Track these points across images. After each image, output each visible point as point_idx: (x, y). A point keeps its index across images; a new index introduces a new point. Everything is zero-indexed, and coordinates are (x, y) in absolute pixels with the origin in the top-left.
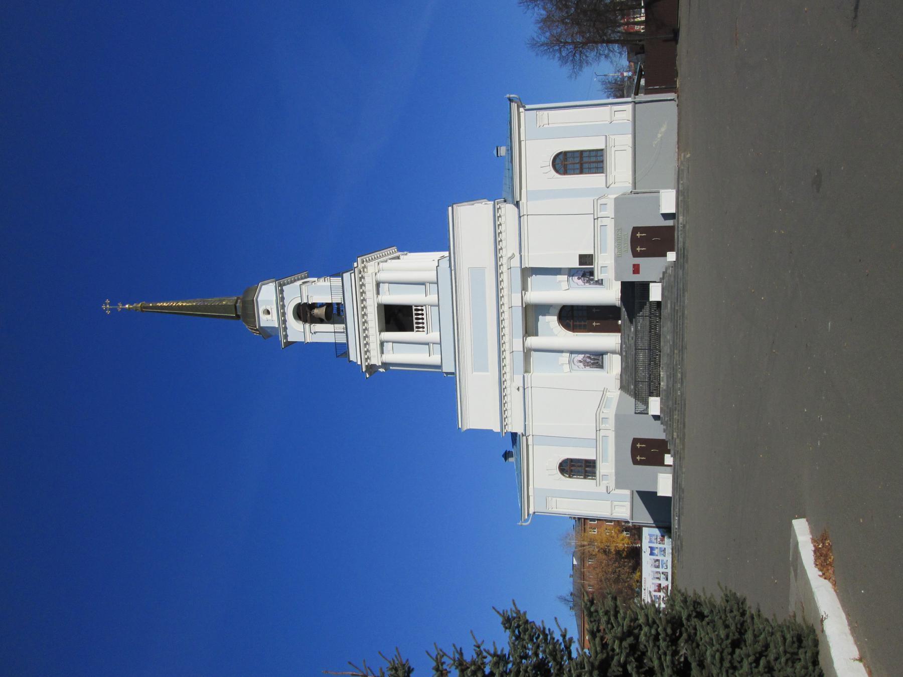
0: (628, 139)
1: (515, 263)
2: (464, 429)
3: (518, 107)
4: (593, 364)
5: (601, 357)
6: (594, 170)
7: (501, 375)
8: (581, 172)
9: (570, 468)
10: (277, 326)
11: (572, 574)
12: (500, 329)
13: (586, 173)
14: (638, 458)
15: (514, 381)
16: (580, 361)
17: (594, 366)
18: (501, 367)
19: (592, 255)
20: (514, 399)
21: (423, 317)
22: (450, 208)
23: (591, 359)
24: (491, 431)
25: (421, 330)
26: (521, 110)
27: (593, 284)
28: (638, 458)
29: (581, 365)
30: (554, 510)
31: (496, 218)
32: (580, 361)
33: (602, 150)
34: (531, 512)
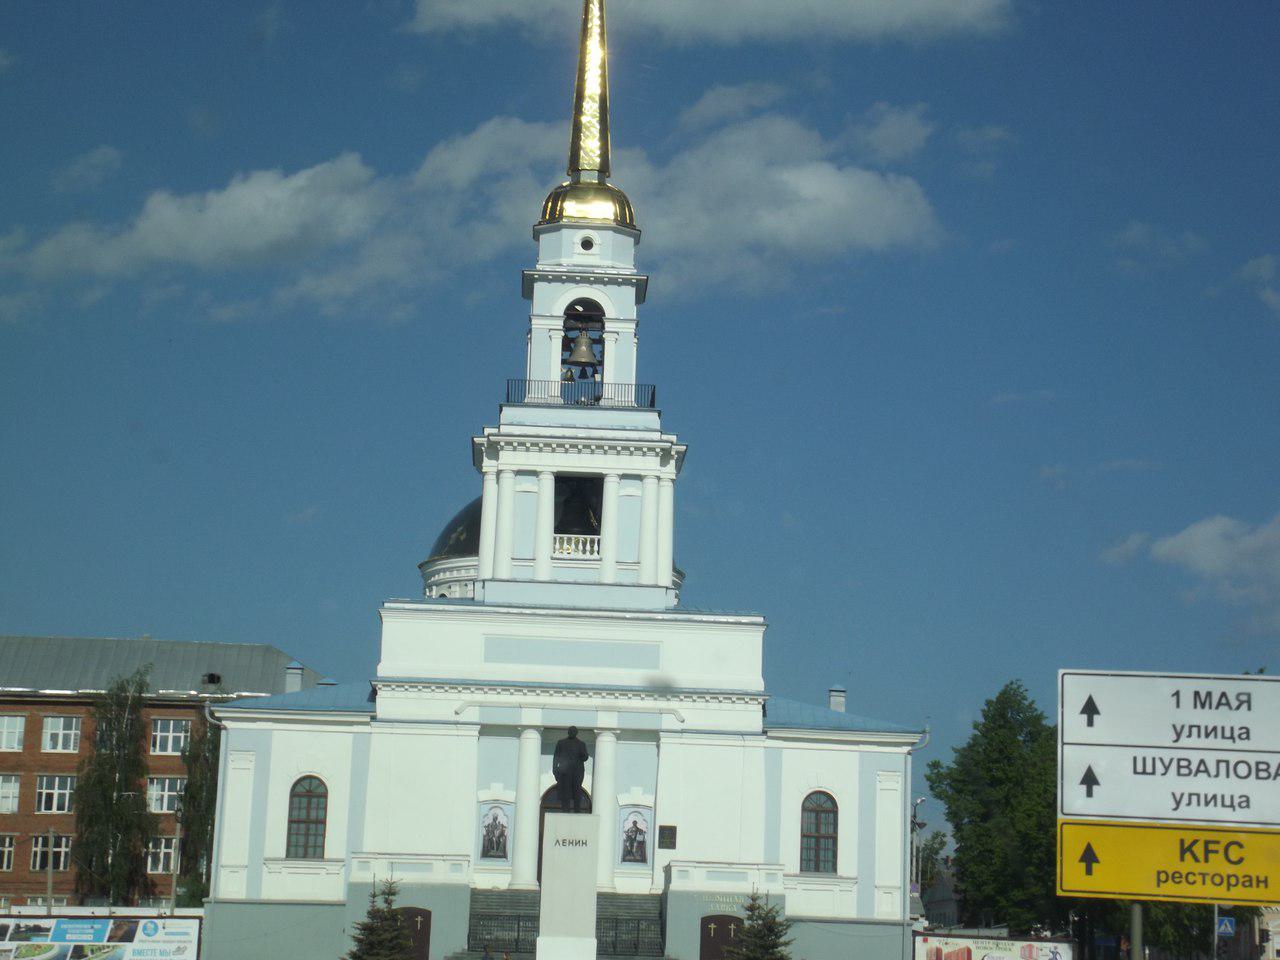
0: (851, 912)
1: (668, 722)
2: (383, 614)
3: (913, 744)
4: (490, 840)
5: (638, 858)
8: (323, 822)
9: (309, 798)
10: (538, 267)
13: (802, 842)
14: (713, 926)
15: (472, 707)
16: (495, 819)
17: (486, 843)
19: (660, 847)
20: (442, 705)
21: (588, 553)
22: (761, 620)
23: (499, 837)
24: (379, 661)
25: (558, 546)
26: (906, 749)
27: (625, 847)
29: (489, 821)
30: (231, 765)
31: (742, 696)
32: (495, 819)
33: (835, 869)
34: (224, 723)
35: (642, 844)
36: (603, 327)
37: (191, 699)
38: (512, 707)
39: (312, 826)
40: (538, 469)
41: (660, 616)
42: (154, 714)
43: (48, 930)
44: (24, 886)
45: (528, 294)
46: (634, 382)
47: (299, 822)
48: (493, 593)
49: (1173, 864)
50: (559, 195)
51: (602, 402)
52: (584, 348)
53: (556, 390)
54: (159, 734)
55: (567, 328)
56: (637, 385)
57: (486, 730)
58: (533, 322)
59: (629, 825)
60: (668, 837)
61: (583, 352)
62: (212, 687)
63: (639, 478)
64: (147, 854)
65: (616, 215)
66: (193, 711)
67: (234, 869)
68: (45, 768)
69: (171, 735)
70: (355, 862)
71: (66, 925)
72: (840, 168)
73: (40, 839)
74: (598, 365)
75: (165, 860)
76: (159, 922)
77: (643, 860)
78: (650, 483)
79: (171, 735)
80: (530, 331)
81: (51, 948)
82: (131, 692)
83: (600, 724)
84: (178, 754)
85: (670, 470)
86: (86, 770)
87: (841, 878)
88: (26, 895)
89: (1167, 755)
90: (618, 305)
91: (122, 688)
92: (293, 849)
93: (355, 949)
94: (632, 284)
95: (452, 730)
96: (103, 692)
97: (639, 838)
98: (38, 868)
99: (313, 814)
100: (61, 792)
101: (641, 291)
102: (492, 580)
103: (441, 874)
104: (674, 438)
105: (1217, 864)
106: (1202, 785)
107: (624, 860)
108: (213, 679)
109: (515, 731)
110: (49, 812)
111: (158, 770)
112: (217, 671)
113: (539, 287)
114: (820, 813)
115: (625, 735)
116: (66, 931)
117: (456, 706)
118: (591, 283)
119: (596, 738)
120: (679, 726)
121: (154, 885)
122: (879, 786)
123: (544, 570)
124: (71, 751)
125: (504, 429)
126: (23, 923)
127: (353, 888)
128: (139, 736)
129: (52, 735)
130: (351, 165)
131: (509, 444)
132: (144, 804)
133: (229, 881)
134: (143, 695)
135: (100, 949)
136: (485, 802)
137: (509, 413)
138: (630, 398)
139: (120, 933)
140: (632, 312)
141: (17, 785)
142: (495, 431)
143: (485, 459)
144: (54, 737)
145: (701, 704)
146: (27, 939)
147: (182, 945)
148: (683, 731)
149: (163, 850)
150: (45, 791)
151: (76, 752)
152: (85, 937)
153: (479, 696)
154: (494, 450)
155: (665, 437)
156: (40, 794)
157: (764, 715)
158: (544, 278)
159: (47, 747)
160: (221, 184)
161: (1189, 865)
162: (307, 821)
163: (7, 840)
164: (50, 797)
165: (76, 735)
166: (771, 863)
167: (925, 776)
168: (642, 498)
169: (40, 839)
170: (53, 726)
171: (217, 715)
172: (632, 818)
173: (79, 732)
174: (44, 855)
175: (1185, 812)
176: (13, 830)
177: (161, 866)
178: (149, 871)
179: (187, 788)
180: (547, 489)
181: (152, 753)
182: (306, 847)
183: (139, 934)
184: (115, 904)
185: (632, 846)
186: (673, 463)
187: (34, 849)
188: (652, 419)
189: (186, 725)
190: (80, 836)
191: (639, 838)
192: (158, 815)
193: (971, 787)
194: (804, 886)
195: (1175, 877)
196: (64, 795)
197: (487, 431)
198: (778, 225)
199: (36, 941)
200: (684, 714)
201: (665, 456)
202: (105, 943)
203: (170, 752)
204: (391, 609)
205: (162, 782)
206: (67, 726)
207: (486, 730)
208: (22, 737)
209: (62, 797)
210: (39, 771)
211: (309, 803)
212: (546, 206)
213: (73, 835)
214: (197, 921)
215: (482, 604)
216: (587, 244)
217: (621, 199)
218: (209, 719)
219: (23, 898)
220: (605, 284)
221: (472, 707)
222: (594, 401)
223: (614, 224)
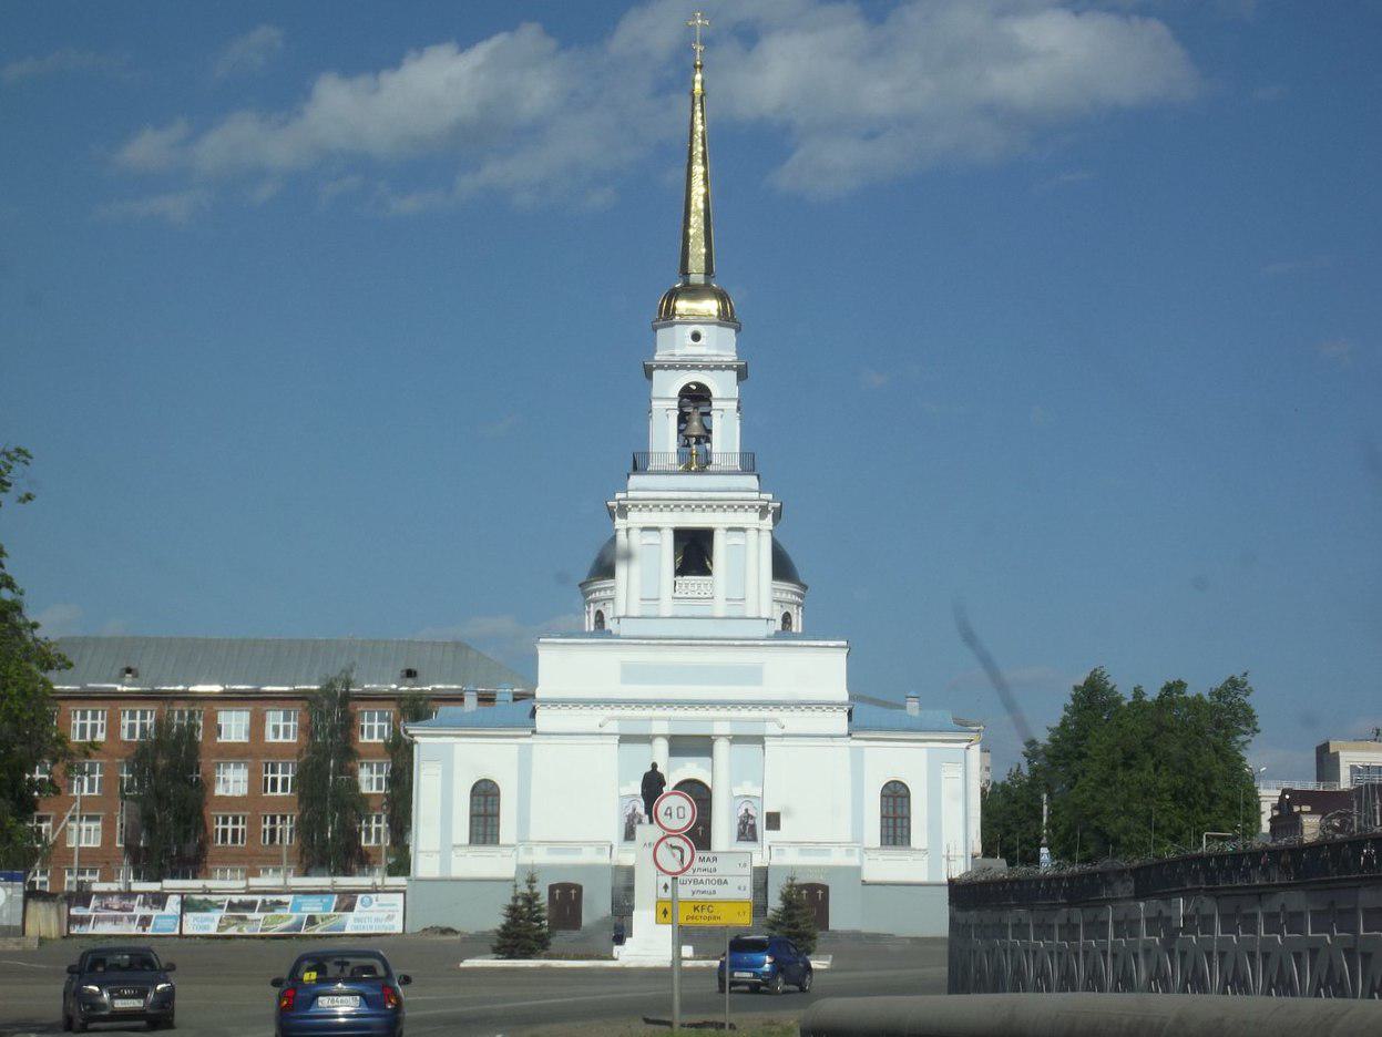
1: (771, 729)
2: (539, 647)
6: (495, 830)
7: (618, 703)
8: (498, 815)
9: (485, 798)
10: (656, 358)
11: (988, 765)
12: (680, 704)
14: (805, 892)
15: (611, 719)
18: (628, 703)
22: (844, 643)
27: (739, 829)
28: (558, 891)
31: (831, 705)
35: (753, 827)
36: (710, 405)
37: (392, 692)
38: (644, 720)
39: (490, 819)
40: (660, 526)
41: (762, 643)
42: (361, 707)
43: (287, 903)
44: (269, 859)
45: (649, 376)
46: (738, 450)
47: (478, 816)
48: (626, 628)
49: (692, 913)
50: (673, 295)
51: (710, 468)
52: (695, 423)
53: (674, 459)
54: (366, 724)
55: (681, 407)
56: (742, 454)
57: (625, 739)
58: (653, 403)
59: (742, 812)
60: (773, 821)
61: (695, 427)
62: (410, 681)
63: (743, 530)
64: (361, 829)
65: (719, 310)
66: (392, 702)
67: (428, 853)
68: (269, 755)
69: (376, 724)
70: (521, 849)
71: (301, 899)
72: (1077, 14)
73: (268, 818)
74: (706, 436)
75: (375, 833)
76: (373, 896)
77: (754, 839)
78: (752, 534)
79: (376, 724)
80: (651, 411)
81: (290, 917)
82: (340, 689)
83: (716, 732)
84: (382, 741)
85: (768, 522)
86: (305, 756)
87: (915, 849)
88: (260, 867)
89: (690, 878)
90: (722, 387)
91: (331, 685)
92: (474, 838)
93: (504, 923)
94: (734, 369)
95: (597, 740)
96: (316, 687)
97: (751, 822)
98: (267, 842)
99: (489, 808)
100: (284, 774)
101: (742, 374)
102: (624, 617)
103: (588, 857)
104: (770, 496)
105: (705, 913)
106: (701, 887)
107: (739, 839)
108: (410, 674)
109: (648, 739)
110: (274, 794)
111: (366, 756)
112: (413, 667)
113: (656, 374)
114: (896, 799)
115: (736, 739)
116: (300, 905)
117: (599, 721)
118: (700, 369)
119: (712, 745)
120: (780, 732)
121: (368, 855)
122: (944, 775)
123: (667, 607)
124: (291, 740)
125: (631, 494)
126: (269, 898)
127: (520, 868)
128: (348, 725)
129: (274, 726)
130: (529, 36)
131: (634, 506)
132: (356, 787)
133: (425, 864)
134: (352, 690)
135: (328, 917)
136: (627, 797)
137: (635, 480)
138: (736, 464)
139: (344, 905)
140: (735, 392)
141: (247, 771)
142: (623, 495)
143: (617, 518)
144: (276, 729)
145: (797, 713)
146: (272, 911)
147: (391, 913)
148: (783, 736)
149: (374, 825)
150: (270, 776)
151: (295, 741)
152: (315, 909)
153: (617, 712)
154: (623, 511)
155: (763, 496)
156: (266, 779)
157: (850, 719)
158: (661, 367)
159: (270, 738)
160: (395, 63)
161: (696, 913)
162: (485, 816)
163: (240, 819)
164: (274, 781)
165: (294, 726)
166: (857, 840)
167: (1024, 753)
168: (745, 547)
169: (268, 818)
170: (274, 718)
171: (410, 732)
172: (744, 807)
173: (297, 724)
174: (273, 832)
175: (696, 896)
176: (245, 810)
177: (373, 839)
178: (363, 844)
179: (393, 771)
180: (668, 540)
181: (361, 741)
182: (485, 835)
183: (358, 906)
184: (335, 874)
185: (745, 829)
186: (770, 516)
187: (263, 826)
188: (751, 481)
189: (389, 715)
190: (302, 815)
191: (751, 822)
192: (369, 796)
193: (1061, 761)
194: (886, 857)
195: (692, 918)
196: (287, 778)
197: (618, 496)
198: (1014, 84)
199: (278, 912)
200: (784, 721)
201: (763, 511)
202: (332, 913)
203: (376, 739)
204: (544, 643)
205: (370, 766)
206: (287, 718)
207: (625, 739)
208: (248, 728)
209: (285, 781)
210: (265, 757)
211: (486, 801)
212: (662, 304)
213: (296, 814)
214: (402, 895)
215: (618, 637)
216: (696, 337)
217: (722, 296)
218: (404, 736)
219: (255, 869)
220: (712, 369)
221: (611, 719)
222: (702, 471)
223: (718, 320)
